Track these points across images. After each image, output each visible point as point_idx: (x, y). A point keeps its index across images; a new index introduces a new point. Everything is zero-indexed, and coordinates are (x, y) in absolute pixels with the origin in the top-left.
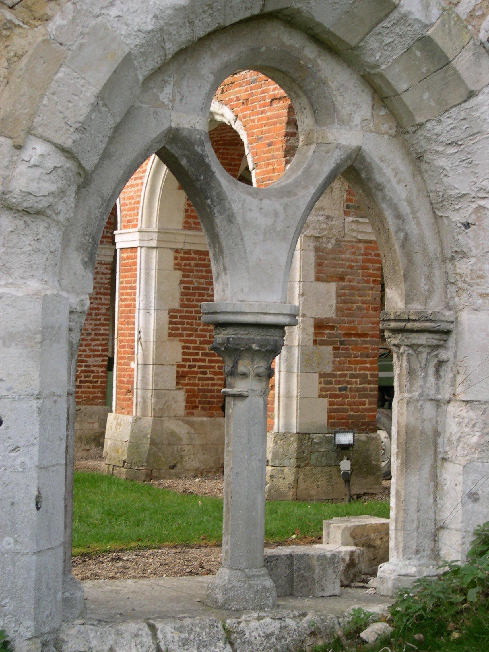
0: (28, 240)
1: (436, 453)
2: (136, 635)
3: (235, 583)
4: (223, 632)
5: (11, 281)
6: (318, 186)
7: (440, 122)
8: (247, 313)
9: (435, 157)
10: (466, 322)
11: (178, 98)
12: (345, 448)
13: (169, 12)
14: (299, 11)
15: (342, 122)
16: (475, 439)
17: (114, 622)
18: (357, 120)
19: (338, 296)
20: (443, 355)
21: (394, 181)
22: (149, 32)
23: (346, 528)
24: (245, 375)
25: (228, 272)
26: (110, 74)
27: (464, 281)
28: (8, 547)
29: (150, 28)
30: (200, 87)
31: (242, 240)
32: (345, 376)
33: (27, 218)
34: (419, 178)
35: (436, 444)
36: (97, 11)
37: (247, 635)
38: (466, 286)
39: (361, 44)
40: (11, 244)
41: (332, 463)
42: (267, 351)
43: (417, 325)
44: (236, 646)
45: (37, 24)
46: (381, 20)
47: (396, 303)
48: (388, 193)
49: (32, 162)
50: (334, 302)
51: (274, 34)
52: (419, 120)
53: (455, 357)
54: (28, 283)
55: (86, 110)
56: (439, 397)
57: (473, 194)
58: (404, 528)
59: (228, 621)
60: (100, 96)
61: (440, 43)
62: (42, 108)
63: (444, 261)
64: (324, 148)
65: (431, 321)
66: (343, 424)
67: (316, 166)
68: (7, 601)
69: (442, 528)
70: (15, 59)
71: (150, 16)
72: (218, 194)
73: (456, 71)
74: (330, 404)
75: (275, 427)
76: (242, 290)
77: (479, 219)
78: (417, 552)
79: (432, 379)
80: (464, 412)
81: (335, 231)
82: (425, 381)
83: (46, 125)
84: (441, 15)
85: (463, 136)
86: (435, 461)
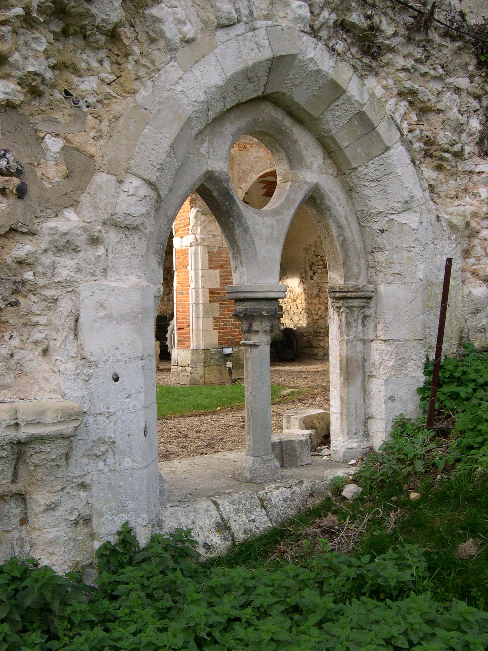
0: (128, 248)
1: (364, 372)
2: (207, 511)
3: (257, 466)
4: (258, 501)
5: (119, 277)
6: (295, 208)
7: (367, 166)
8: (259, 292)
9: (363, 189)
10: (383, 291)
11: (212, 150)
12: (228, 355)
13: (213, 89)
14: (284, 95)
15: (308, 167)
16: (392, 363)
17: (189, 501)
18: (315, 166)
19: (221, 276)
20: (368, 312)
21: (337, 204)
22: (201, 102)
23: (301, 418)
24: (257, 332)
25: (244, 265)
26: (178, 131)
27: (381, 266)
28: (128, 465)
29: (202, 100)
30: (224, 144)
31: (254, 244)
32: (226, 318)
33: (127, 233)
34: (350, 203)
35: (364, 367)
36: (168, 87)
37: (273, 501)
38: (382, 269)
39: (321, 116)
40: (117, 251)
41: (222, 364)
42: (271, 315)
43: (354, 294)
44: (268, 510)
45: (127, 95)
46: (335, 101)
47: (337, 281)
48: (333, 212)
49: (131, 192)
50: (219, 280)
51: (267, 110)
52: (354, 165)
53: (376, 313)
54: (130, 278)
55: (164, 156)
56: (365, 338)
57: (387, 212)
58: (347, 419)
59: (259, 493)
60: (172, 147)
61: (370, 116)
62: (135, 154)
63: (366, 253)
64: (296, 184)
65: (362, 291)
66: (226, 343)
67: (293, 195)
68: (129, 502)
69: (370, 418)
70: (114, 120)
71: (202, 92)
72: (238, 214)
73: (379, 134)
74: (219, 333)
75: (191, 347)
76: (254, 277)
77: (390, 227)
78: (356, 433)
79: (360, 327)
80: (383, 346)
81: (218, 242)
82: (357, 329)
83: (138, 166)
84: (370, 98)
85: (381, 175)
86: (364, 377)
